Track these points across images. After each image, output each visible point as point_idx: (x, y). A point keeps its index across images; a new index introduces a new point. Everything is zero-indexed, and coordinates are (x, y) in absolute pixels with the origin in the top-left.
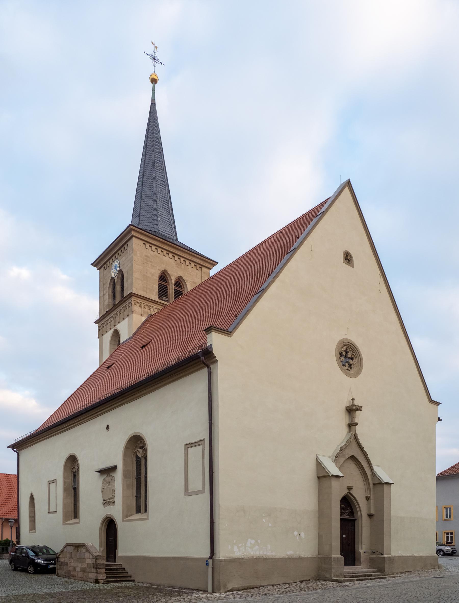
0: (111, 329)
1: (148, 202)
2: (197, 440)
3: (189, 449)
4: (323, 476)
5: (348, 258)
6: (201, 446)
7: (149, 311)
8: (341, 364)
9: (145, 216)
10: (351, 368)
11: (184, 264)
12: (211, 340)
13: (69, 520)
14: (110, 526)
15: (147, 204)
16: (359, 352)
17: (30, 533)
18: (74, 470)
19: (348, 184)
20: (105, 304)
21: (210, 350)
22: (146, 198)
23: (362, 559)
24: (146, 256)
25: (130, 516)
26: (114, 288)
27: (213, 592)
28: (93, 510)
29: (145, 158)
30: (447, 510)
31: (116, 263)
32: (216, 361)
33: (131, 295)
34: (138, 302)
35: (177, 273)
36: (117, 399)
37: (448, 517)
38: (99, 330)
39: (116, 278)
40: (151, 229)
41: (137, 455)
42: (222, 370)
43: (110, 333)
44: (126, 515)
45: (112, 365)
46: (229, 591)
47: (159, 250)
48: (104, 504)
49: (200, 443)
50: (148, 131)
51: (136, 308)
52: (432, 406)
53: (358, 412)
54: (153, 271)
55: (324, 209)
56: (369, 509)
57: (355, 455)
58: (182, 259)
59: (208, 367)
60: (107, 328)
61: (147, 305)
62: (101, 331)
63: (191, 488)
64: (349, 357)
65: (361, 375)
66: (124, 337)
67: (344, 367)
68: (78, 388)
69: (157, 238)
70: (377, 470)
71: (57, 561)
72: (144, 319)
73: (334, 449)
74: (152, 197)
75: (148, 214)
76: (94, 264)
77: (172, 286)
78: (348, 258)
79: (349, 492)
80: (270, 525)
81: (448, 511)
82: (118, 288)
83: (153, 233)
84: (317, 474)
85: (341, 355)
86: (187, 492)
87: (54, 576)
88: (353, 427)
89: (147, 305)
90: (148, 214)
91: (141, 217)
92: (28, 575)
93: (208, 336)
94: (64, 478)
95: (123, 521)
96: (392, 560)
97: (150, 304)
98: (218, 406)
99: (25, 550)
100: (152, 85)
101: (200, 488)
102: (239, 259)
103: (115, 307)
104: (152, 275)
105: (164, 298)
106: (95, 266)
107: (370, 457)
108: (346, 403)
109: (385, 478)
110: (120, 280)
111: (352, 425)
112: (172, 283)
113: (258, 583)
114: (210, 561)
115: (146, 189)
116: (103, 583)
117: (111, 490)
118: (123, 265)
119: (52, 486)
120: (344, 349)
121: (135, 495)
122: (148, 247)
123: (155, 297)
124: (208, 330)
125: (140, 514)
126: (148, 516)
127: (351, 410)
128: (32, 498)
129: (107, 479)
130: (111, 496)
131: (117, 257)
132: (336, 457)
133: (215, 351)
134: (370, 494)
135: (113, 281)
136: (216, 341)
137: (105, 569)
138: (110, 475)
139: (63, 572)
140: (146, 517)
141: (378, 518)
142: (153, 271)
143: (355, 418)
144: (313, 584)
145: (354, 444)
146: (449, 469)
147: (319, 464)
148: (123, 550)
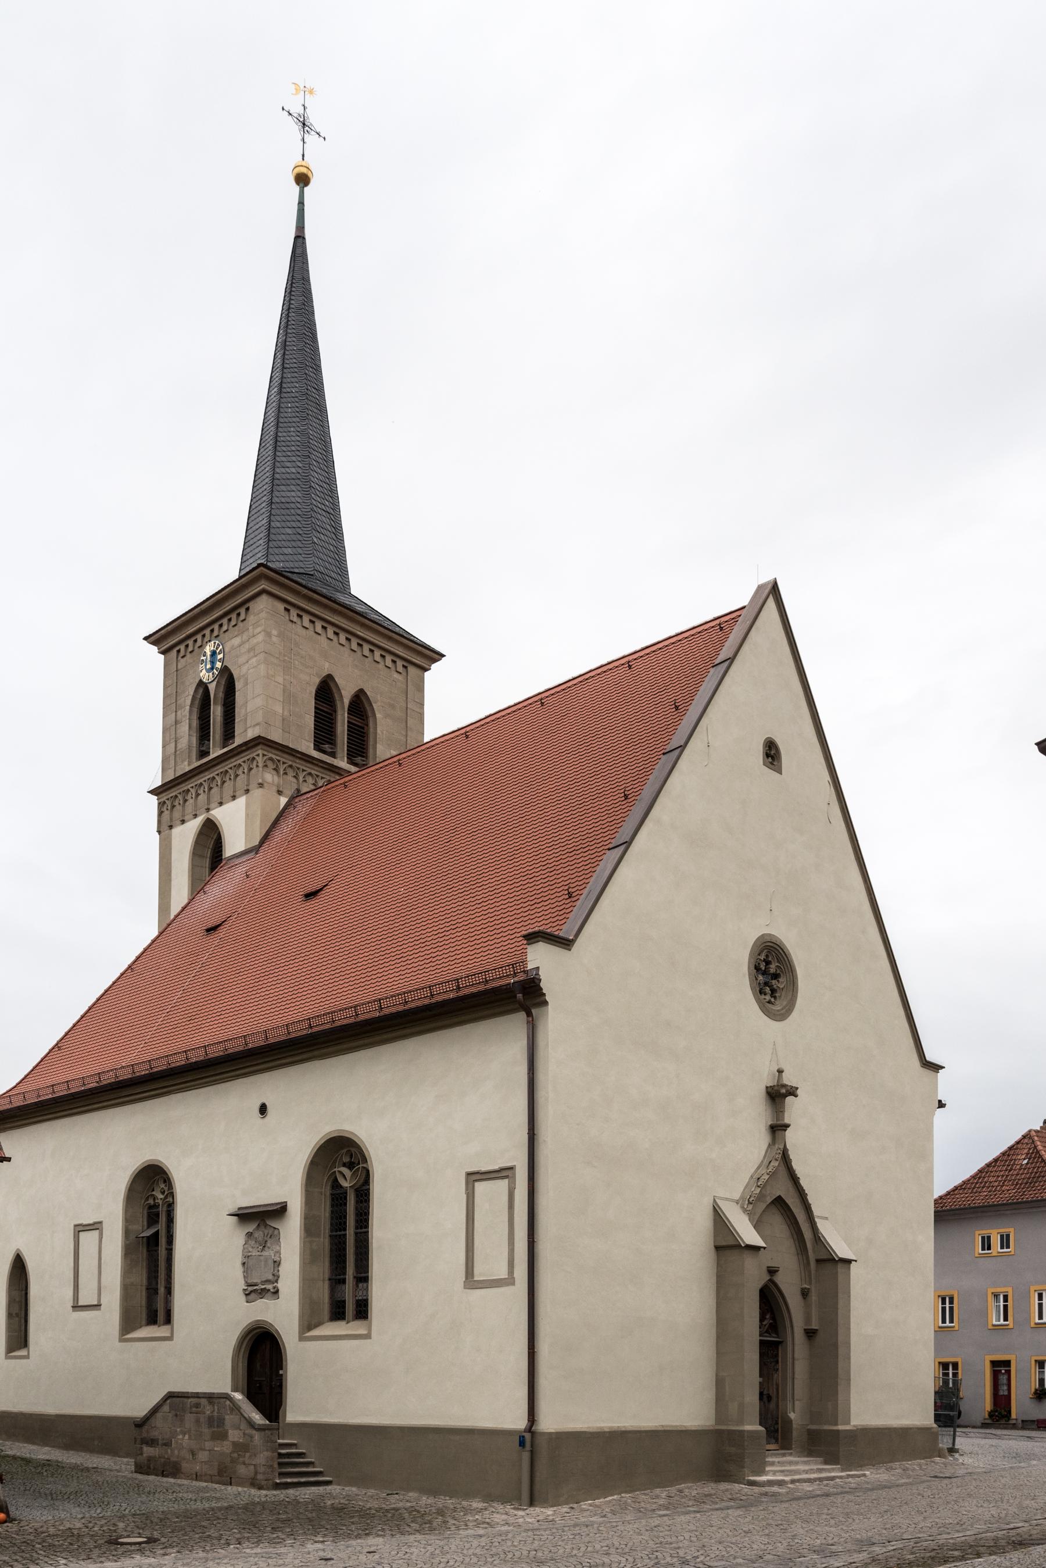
0: (195, 816)
1: (289, 494)
2: (496, 1167)
3: (477, 1184)
4: (726, 1246)
5: (772, 753)
6: (506, 1181)
7: (294, 780)
10: (775, 998)
17: (7, 1357)
18: (151, 1201)
19: (774, 590)
22: (283, 482)
23: (795, 1434)
30: (944, 1302)
32: (546, 1003)
34: (271, 759)
37: (948, 1324)
38: (160, 813)
39: (212, 687)
41: (336, 1180)
42: (555, 1020)
43: (193, 826)
44: (308, 1324)
48: (247, 1295)
49: (504, 1174)
53: (789, 1099)
56: (808, 1319)
57: (783, 1200)
59: (529, 1014)
61: (291, 766)
62: (166, 813)
64: (772, 973)
66: (234, 842)
67: (763, 996)
72: (283, 801)
74: (299, 482)
75: (288, 524)
76: (152, 639)
77: (343, 715)
78: (772, 752)
79: (770, 1280)
81: (947, 1305)
82: (216, 712)
85: (757, 968)
86: (471, 1281)
88: (779, 1133)
91: (272, 530)
94: (128, 1220)
95: (302, 1338)
100: (297, 189)
101: (503, 1274)
105: (327, 747)
106: (154, 643)
107: (811, 1199)
108: (767, 1079)
109: (842, 1250)
110: (221, 695)
111: (778, 1129)
115: (284, 459)
117: (271, 1263)
119: (88, 1239)
121: (327, 1276)
122: (295, 619)
123: (307, 746)
124: (532, 937)
125: (342, 1323)
127: (778, 1095)
130: (271, 1277)
133: (546, 985)
134: (810, 1283)
135: (201, 691)
136: (540, 958)
138: (266, 1225)
141: (827, 1340)
143: (783, 1112)
145: (783, 1173)
146: (948, 1193)
147: (719, 1220)
148: (299, 1408)
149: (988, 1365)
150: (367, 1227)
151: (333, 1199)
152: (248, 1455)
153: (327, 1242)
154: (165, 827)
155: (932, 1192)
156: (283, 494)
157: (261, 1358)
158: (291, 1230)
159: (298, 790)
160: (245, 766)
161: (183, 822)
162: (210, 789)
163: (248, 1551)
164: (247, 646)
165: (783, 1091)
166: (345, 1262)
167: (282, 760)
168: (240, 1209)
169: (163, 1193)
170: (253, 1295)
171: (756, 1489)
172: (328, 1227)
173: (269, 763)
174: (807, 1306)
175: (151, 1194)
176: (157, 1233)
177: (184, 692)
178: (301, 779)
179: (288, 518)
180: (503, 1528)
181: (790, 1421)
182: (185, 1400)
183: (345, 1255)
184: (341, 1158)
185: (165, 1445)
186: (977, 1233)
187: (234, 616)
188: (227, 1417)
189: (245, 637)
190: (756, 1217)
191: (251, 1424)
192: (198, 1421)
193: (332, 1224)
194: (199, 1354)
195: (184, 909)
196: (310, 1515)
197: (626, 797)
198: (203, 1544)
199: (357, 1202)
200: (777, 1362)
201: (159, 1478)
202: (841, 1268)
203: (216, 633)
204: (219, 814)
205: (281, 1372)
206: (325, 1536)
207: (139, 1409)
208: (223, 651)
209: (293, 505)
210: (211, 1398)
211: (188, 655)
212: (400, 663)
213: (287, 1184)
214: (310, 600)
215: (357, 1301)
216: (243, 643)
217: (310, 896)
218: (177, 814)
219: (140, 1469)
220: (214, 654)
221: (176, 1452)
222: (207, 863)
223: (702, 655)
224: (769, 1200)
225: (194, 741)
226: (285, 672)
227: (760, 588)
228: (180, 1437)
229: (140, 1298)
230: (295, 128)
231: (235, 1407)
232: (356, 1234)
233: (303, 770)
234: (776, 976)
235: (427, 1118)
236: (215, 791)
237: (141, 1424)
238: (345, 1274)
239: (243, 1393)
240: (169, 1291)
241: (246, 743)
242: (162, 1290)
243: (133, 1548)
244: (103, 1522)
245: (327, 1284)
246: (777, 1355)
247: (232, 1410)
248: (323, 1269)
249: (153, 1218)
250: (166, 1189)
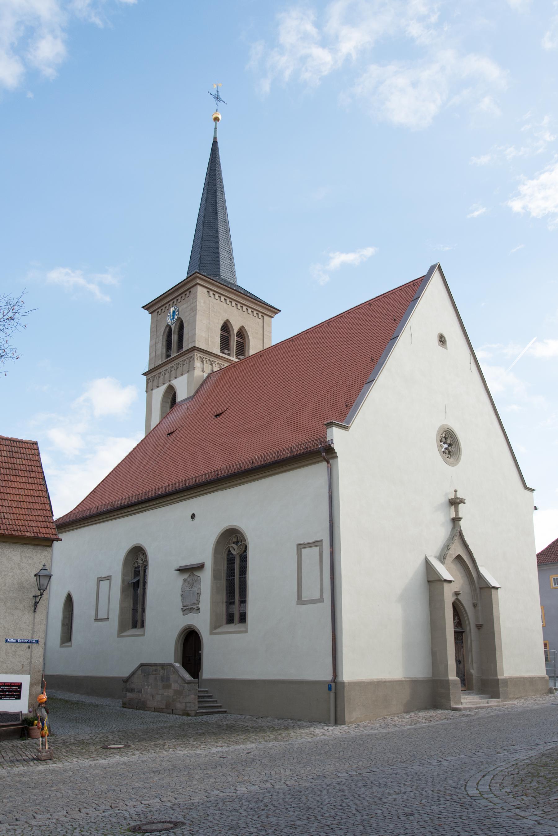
0: (164, 384)
2: (313, 541)
3: (303, 550)
4: (432, 581)
5: (442, 340)
6: (318, 548)
10: (451, 455)
11: (246, 313)
12: (332, 435)
14: (190, 642)
18: (136, 565)
23: (474, 682)
25: (219, 627)
32: (337, 457)
33: (194, 349)
38: (147, 383)
39: (173, 327)
41: (229, 551)
42: (343, 463)
44: (215, 627)
49: (316, 544)
51: (198, 364)
62: (150, 383)
63: (305, 596)
64: (449, 443)
65: (461, 463)
66: (181, 396)
69: (221, 286)
70: (482, 570)
82: (175, 338)
84: (427, 578)
86: (300, 600)
88: (456, 522)
93: (328, 431)
94: (124, 575)
95: (211, 634)
97: (213, 359)
100: (214, 123)
101: (317, 596)
105: (226, 351)
106: (146, 309)
107: (475, 556)
109: (494, 583)
110: (177, 330)
117: (196, 594)
119: (104, 585)
120: (444, 435)
124: (330, 425)
128: (69, 600)
130: (196, 602)
133: (336, 447)
135: (168, 329)
138: (194, 575)
145: (457, 541)
150: (245, 574)
151: (228, 561)
152: (182, 697)
154: (149, 389)
157: (190, 645)
158: (206, 578)
159: (212, 370)
160: (188, 361)
161: (158, 387)
162: (171, 371)
163: (179, 752)
164: (189, 308)
165: (459, 501)
166: (234, 593)
167: (205, 357)
168: (180, 567)
169: (142, 560)
170: (186, 611)
171: (458, 713)
172: (225, 575)
175: (137, 562)
176: (138, 581)
180: (321, 737)
181: (472, 675)
182: (150, 667)
183: (234, 590)
185: (138, 692)
187: (183, 295)
188: (171, 676)
189: (189, 304)
191: (184, 680)
192: (156, 678)
193: (227, 573)
194: (159, 642)
195: (157, 425)
196: (214, 731)
197: (373, 360)
198: (155, 748)
199: (240, 562)
200: (463, 642)
201: (135, 711)
202: (493, 591)
203: (175, 303)
204: (175, 383)
205: (200, 652)
206: (223, 743)
207: (126, 673)
208: (178, 311)
210: (163, 666)
213: (204, 552)
214: (219, 287)
215: (240, 613)
216: (187, 307)
218: (155, 383)
219: (124, 705)
220: (174, 312)
221: (144, 696)
222: (169, 405)
223: (411, 292)
225: (164, 351)
228: (147, 687)
230: (214, 100)
231: (176, 671)
232: (240, 578)
236: (173, 372)
237: (126, 681)
238: (234, 599)
239: (180, 663)
240: (143, 610)
241: (188, 350)
242: (140, 610)
243: (116, 751)
244: (102, 735)
245: (225, 604)
246: (462, 639)
247: (174, 672)
248: (223, 596)
249: (137, 573)
250: (144, 558)
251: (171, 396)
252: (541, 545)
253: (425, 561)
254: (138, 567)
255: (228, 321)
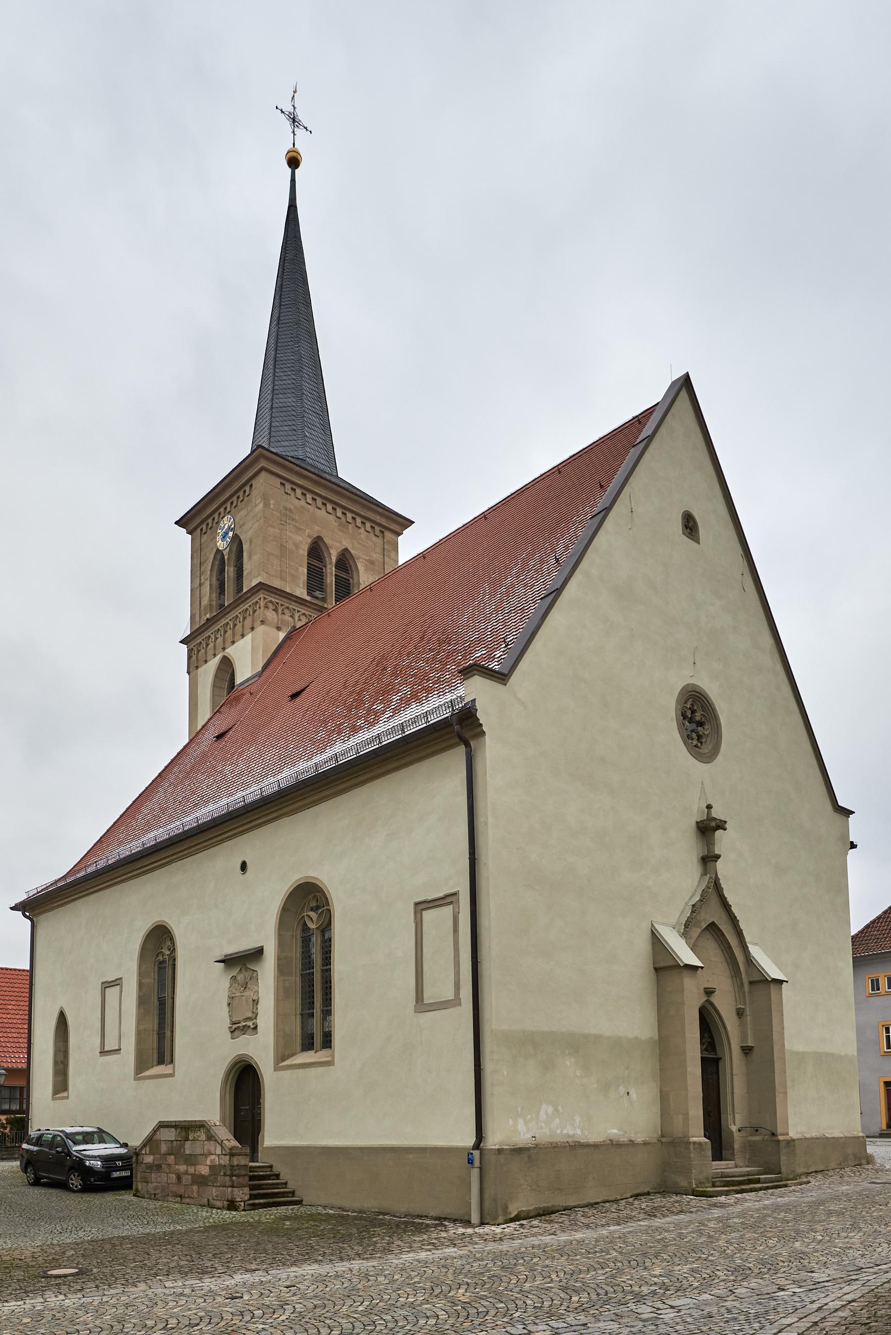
0: (215, 655)
2: (441, 895)
3: (424, 913)
4: (664, 967)
5: (690, 525)
6: (451, 906)
7: (290, 619)
8: (685, 733)
9: (281, 428)
10: (701, 743)
13: (147, 1069)
14: (244, 1082)
15: (285, 405)
16: (714, 710)
17: (53, 1099)
18: (161, 958)
19: (685, 383)
20: (203, 604)
21: (473, 711)
23: (736, 1146)
24: (286, 508)
25: (289, 1057)
26: (222, 571)
27: (482, 1224)
28: (205, 1048)
29: (280, 313)
31: (227, 522)
35: (340, 543)
36: (268, 806)
38: (189, 657)
40: (292, 454)
41: (305, 924)
42: (492, 750)
44: (282, 1057)
45: (227, 732)
46: (512, 1220)
47: (309, 496)
48: (232, 1032)
50: (285, 260)
52: (838, 817)
53: (719, 833)
54: (298, 538)
55: (647, 431)
56: (744, 1036)
57: (715, 922)
58: (349, 515)
59: (467, 745)
60: (206, 653)
61: (288, 608)
62: (194, 657)
64: (697, 719)
65: (720, 757)
66: (243, 672)
68: (153, 778)
70: (755, 951)
71: (137, 1163)
72: (282, 635)
73: (679, 910)
74: (293, 390)
75: (285, 423)
76: (181, 523)
77: (331, 569)
79: (708, 1001)
80: (578, 1073)
83: (298, 462)
84: (654, 963)
85: (684, 716)
86: (420, 1003)
87: (127, 1197)
89: (288, 608)
90: (285, 423)
92: (73, 1196)
94: (141, 975)
96: (791, 1143)
98: (486, 823)
99: (59, 1138)
100: (290, 170)
101: (450, 995)
102: (475, 521)
103: (223, 610)
104: (297, 546)
105: (317, 594)
107: (742, 925)
108: (696, 814)
109: (774, 972)
110: (233, 556)
111: (708, 860)
112: (331, 563)
113: (560, 1201)
114: (476, 1153)
115: (281, 374)
116: (244, 1210)
118: (240, 527)
121: (299, 1011)
123: (301, 592)
125: (312, 1053)
126: (333, 1056)
127: (708, 828)
128: (62, 1021)
129: (240, 978)
130: (250, 1015)
131: (228, 509)
132: (686, 926)
134: (745, 1004)
135: (219, 557)
137: (247, 1178)
139: (151, 1186)
140: (329, 1059)
141: (762, 1054)
142: (298, 538)
143: (713, 844)
144: (658, 1201)
145: (714, 900)
148: (274, 1135)
149: (882, 1085)
153: (298, 980)
155: (846, 922)
156: (281, 400)
158: (267, 972)
159: (294, 627)
167: (280, 602)
170: (237, 1032)
172: (299, 966)
173: (270, 605)
174: (742, 1026)
177: (205, 561)
178: (297, 618)
179: (286, 419)
184: (309, 904)
186: (867, 977)
187: (241, 493)
190: (692, 941)
202: (773, 988)
204: (231, 651)
209: (289, 409)
211: (209, 531)
212: (377, 529)
213: (264, 933)
216: (249, 513)
217: (294, 696)
224: (704, 926)
226: (283, 538)
227: (674, 384)
229: (152, 1041)
233: (298, 611)
234: (701, 724)
235: (380, 858)
248: (295, 1004)
251: (228, 677)
252: (859, 919)
253: (650, 932)
254: (164, 962)
255: (319, 538)
